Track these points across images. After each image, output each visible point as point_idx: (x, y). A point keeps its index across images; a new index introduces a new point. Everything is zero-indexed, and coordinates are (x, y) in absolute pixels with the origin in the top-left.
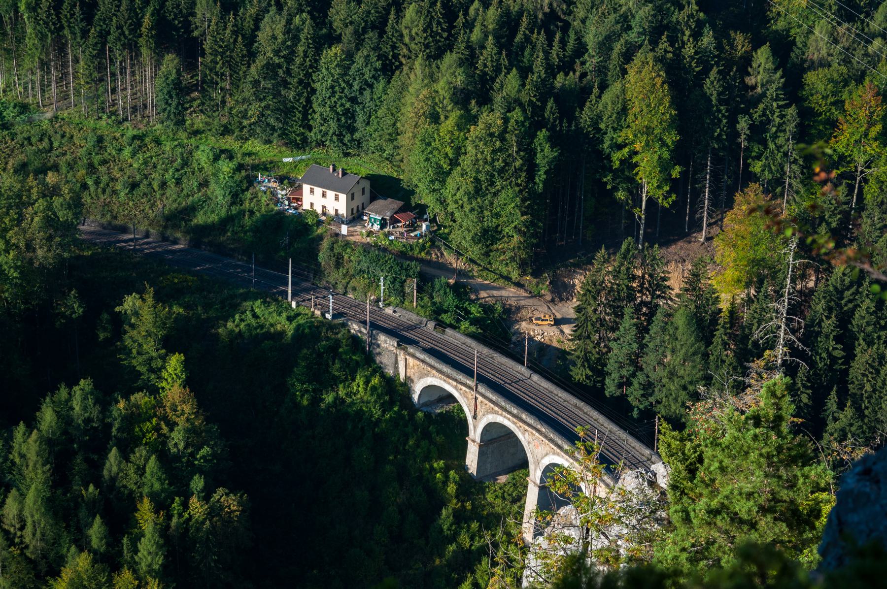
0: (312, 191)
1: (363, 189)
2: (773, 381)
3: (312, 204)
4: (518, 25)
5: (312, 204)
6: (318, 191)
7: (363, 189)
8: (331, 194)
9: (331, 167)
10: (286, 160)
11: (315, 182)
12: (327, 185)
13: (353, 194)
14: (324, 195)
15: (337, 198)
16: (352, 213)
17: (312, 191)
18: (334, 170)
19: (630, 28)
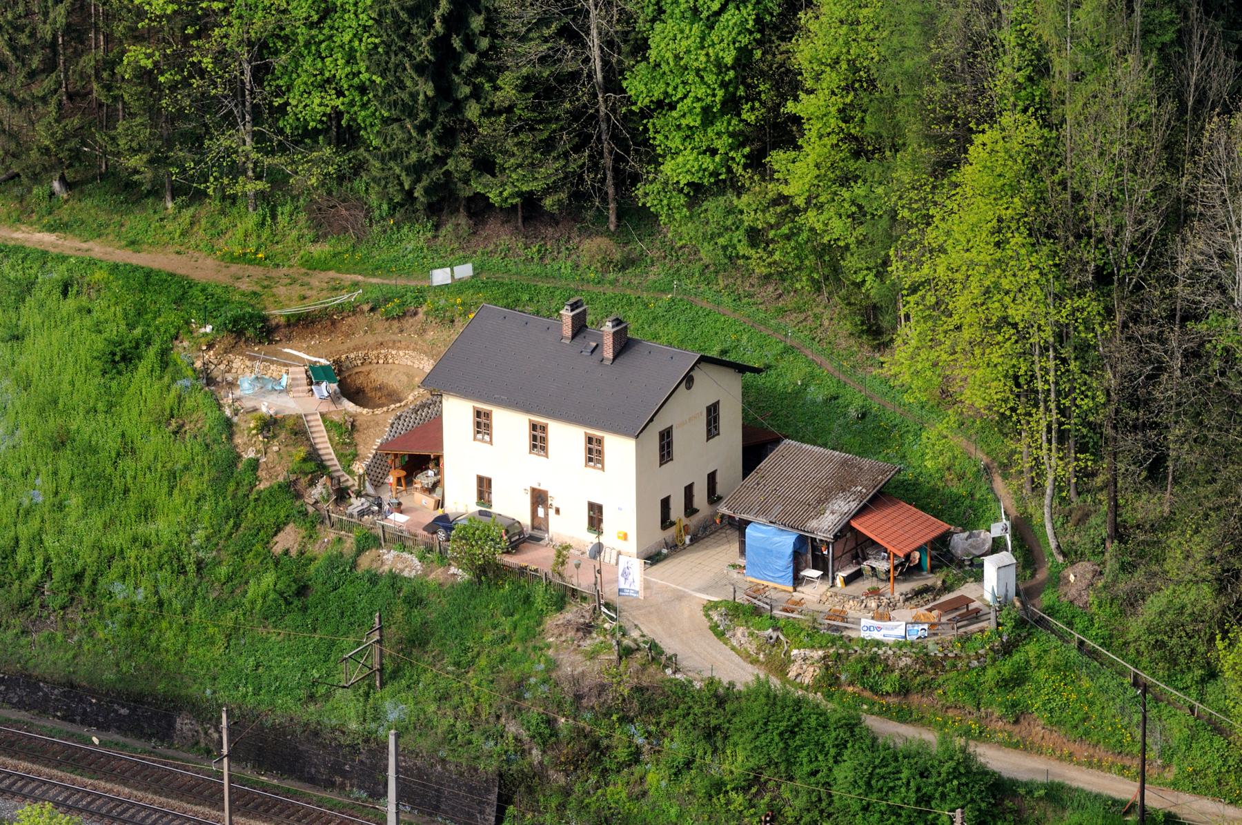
0: (482, 424)
1: (713, 412)
2: (606, 154)
3: (484, 485)
4: (619, 218)
5: (484, 485)
6: (511, 425)
7: (713, 412)
8: (567, 438)
9: (567, 314)
10: (441, 277)
11: (493, 386)
12: (544, 401)
13: (666, 437)
14: (538, 441)
15: (594, 453)
16: (666, 522)
17: (482, 424)
18: (580, 327)
19: (784, 132)
